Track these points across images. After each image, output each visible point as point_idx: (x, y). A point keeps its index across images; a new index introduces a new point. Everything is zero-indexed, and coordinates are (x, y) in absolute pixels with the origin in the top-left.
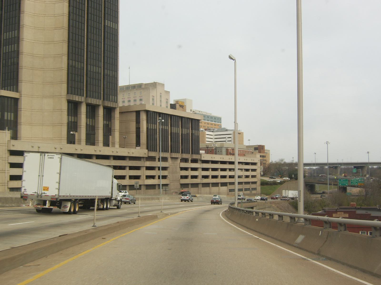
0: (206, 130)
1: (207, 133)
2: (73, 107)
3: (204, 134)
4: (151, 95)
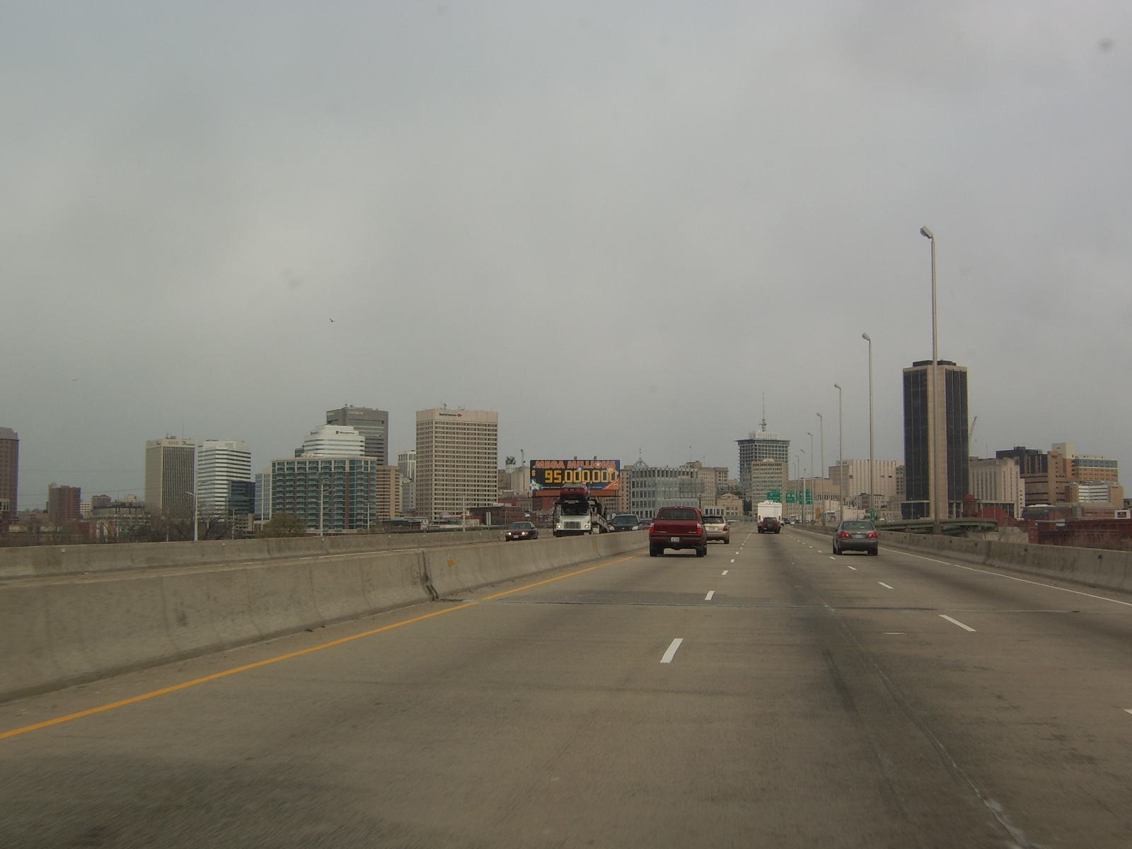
0: (1080, 483)
1: (1080, 487)
2: (950, 505)
3: (1077, 489)
4: (1003, 470)
